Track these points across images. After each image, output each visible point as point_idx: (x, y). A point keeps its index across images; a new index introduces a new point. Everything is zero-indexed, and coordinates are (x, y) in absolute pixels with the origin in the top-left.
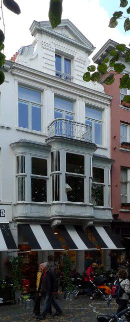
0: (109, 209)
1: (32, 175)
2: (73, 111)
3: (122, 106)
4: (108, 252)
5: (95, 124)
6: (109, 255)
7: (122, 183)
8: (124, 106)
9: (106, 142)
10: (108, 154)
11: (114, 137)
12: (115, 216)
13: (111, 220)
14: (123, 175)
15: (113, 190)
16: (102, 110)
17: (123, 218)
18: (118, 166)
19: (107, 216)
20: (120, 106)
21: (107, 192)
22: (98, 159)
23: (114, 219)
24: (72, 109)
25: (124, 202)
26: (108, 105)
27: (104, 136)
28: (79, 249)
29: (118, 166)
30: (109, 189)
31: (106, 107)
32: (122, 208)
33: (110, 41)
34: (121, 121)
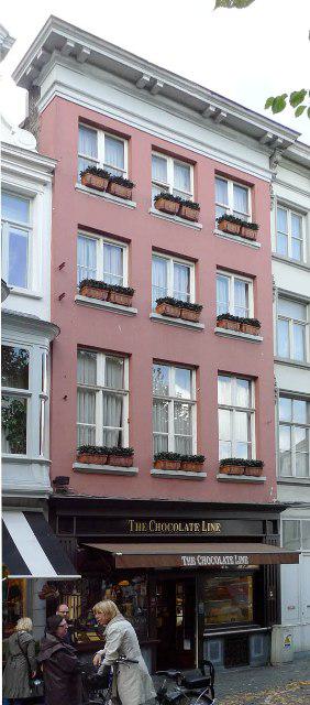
0: (41, 463)
1: (6, 388)
2: (27, 221)
3: (84, 187)
4: (39, 588)
5: (12, 235)
6: (41, 597)
7: (81, 391)
8: (224, 231)
9: (39, 278)
10: (43, 312)
11: (60, 268)
12: (59, 482)
13: (44, 493)
14: (82, 367)
15: (54, 417)
16: (31, 197)
17: (81, 488)
18: (68, 345)
19: (38, 481)
20: (153, 210)
21: (37, 414)
22: (36, 328)
23: (58, 492)
24: (27, 210)
25: (87, 444)
26: (45, 184)
27: (34, 266)
28: (34, 575)
29: (68, 345)
30: (45, 406)
31: (40, 188)
32: (79, 459)
33: (54, 21)
34: (154, 249)
